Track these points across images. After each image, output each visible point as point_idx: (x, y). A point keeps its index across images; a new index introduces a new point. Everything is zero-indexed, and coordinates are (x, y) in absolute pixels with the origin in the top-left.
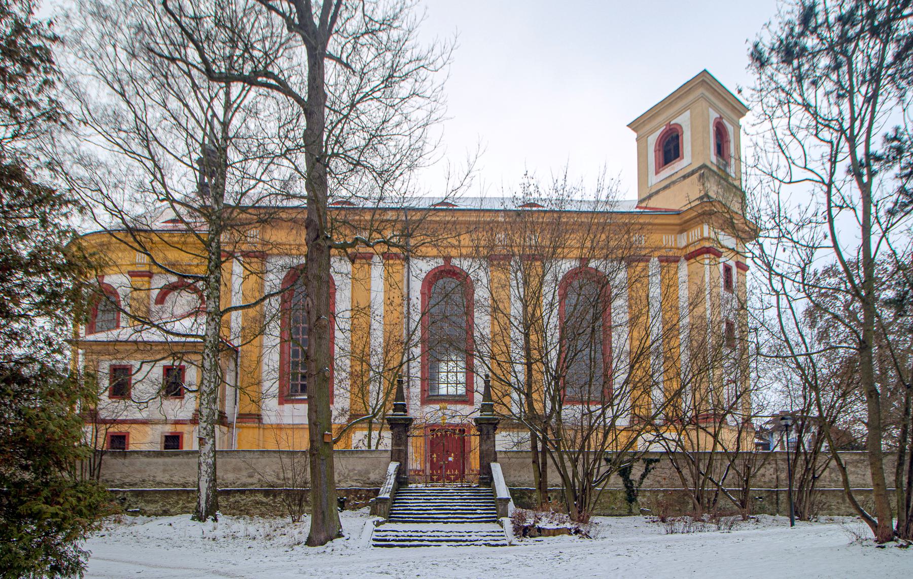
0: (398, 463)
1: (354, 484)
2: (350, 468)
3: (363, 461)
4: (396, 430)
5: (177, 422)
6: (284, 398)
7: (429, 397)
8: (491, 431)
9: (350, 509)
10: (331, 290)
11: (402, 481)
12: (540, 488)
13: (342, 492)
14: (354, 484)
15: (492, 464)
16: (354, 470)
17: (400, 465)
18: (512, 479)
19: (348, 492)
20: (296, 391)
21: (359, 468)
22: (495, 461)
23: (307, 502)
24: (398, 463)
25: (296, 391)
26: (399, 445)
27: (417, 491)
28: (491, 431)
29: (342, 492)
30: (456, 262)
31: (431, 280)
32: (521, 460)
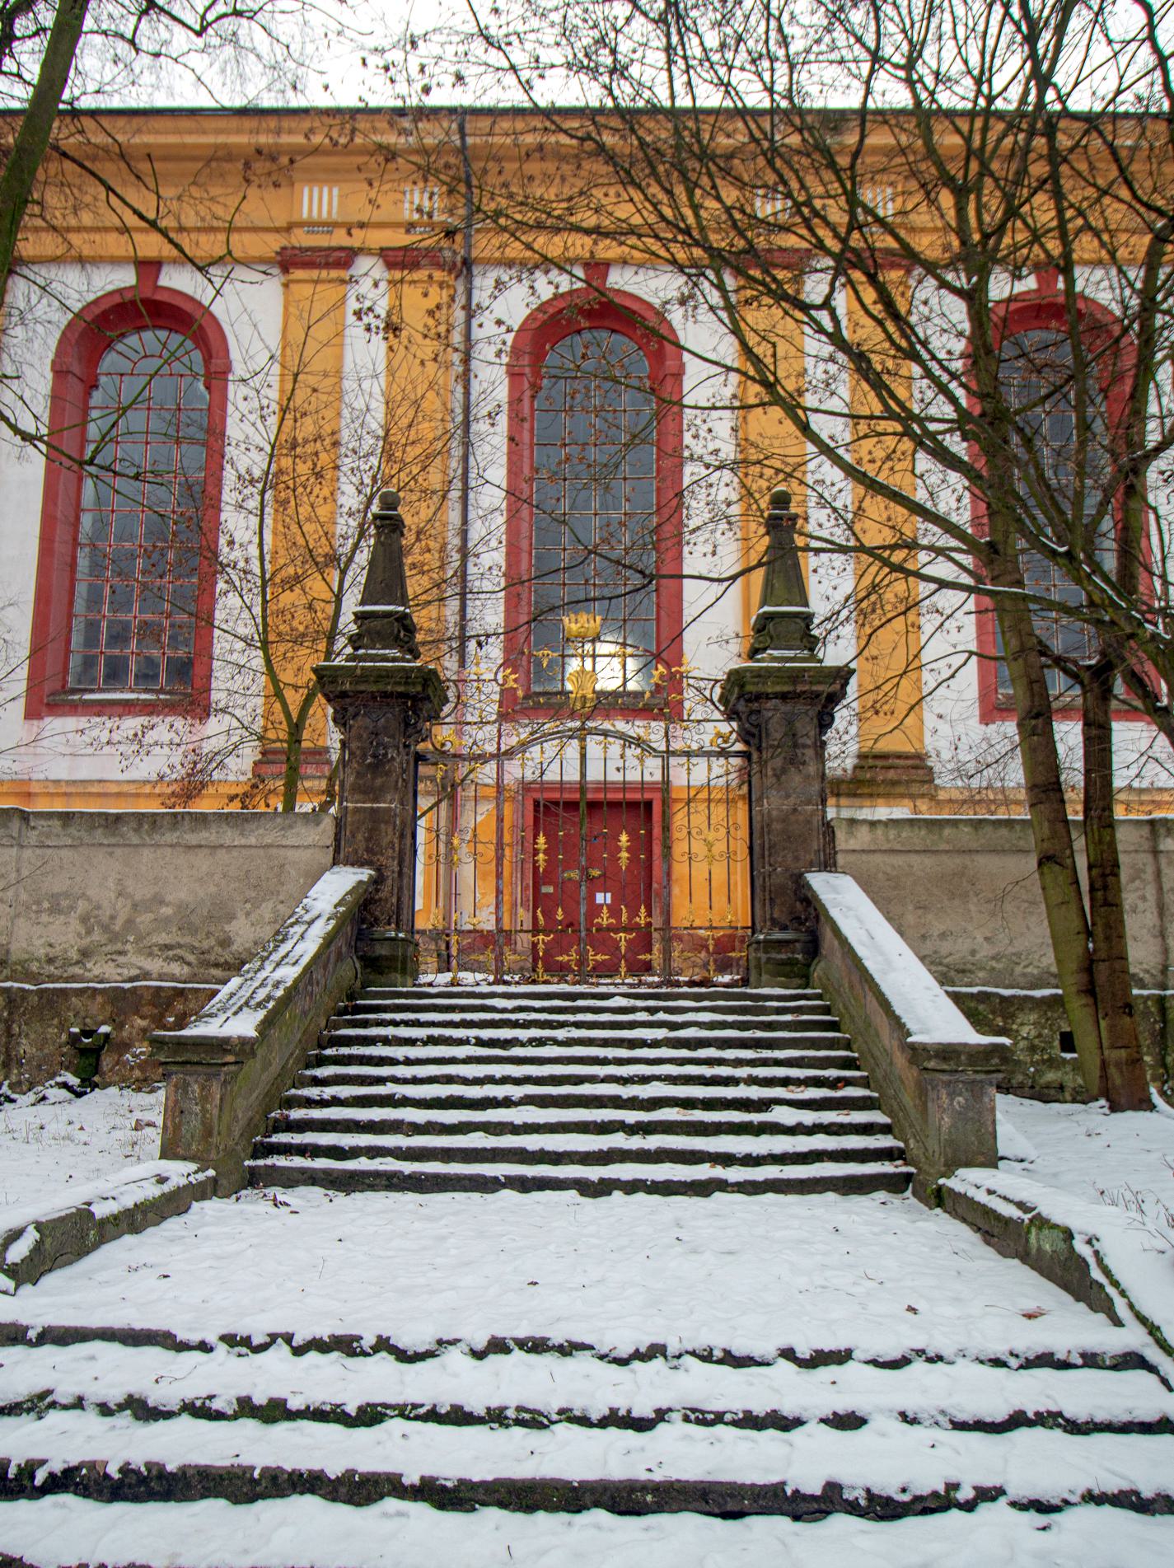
0: (365, 874)
1: (154, 965)
2: (142, 892)
7: (537, 701)
9: (125, 1083)
12: (1090, 990)
13: (95, 1006)
14: (154, 965)
15: (818, 881)
17: (377, 882)
19: (122, 1002)
20: (93, 680)
21: (180, 893)
22: (828, 864)
24: (365, 874)
25: (93, 680)
27: (450, 1000)
29: (95, 1006)
30: (619, 279)
31: (546, 330)
32: (952, 863)
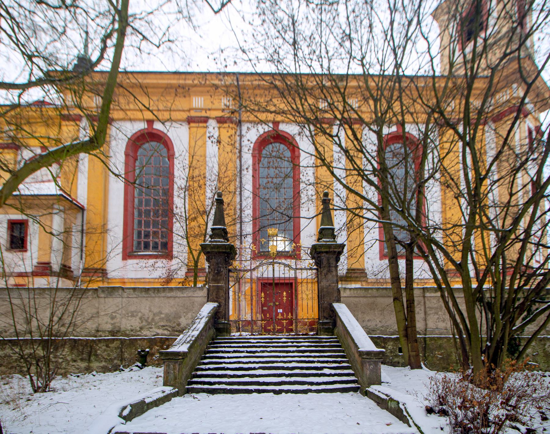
0: (216, 304)
1: (160, 331)
2: (156, 310)
3: (172, 302)
4: (214, 260)
5: (21, 275)
6: (127, 255)
8: (332, 261)
9: (153, 365)
10: (171, 152)
11: (218, 325)
12: (406, 336)
13: (145, 343)
14: (160, 331)
15: (336, 305)
16: (161, 313)
17: (219, 307)
18: (372, 325)
20: (141, 249)
21: (166, 311)
22: (339, 301)
23: (96, 355)
24: (216, 304)
26: (217, 281)
28: (332, 261)
31: (262, 143)
